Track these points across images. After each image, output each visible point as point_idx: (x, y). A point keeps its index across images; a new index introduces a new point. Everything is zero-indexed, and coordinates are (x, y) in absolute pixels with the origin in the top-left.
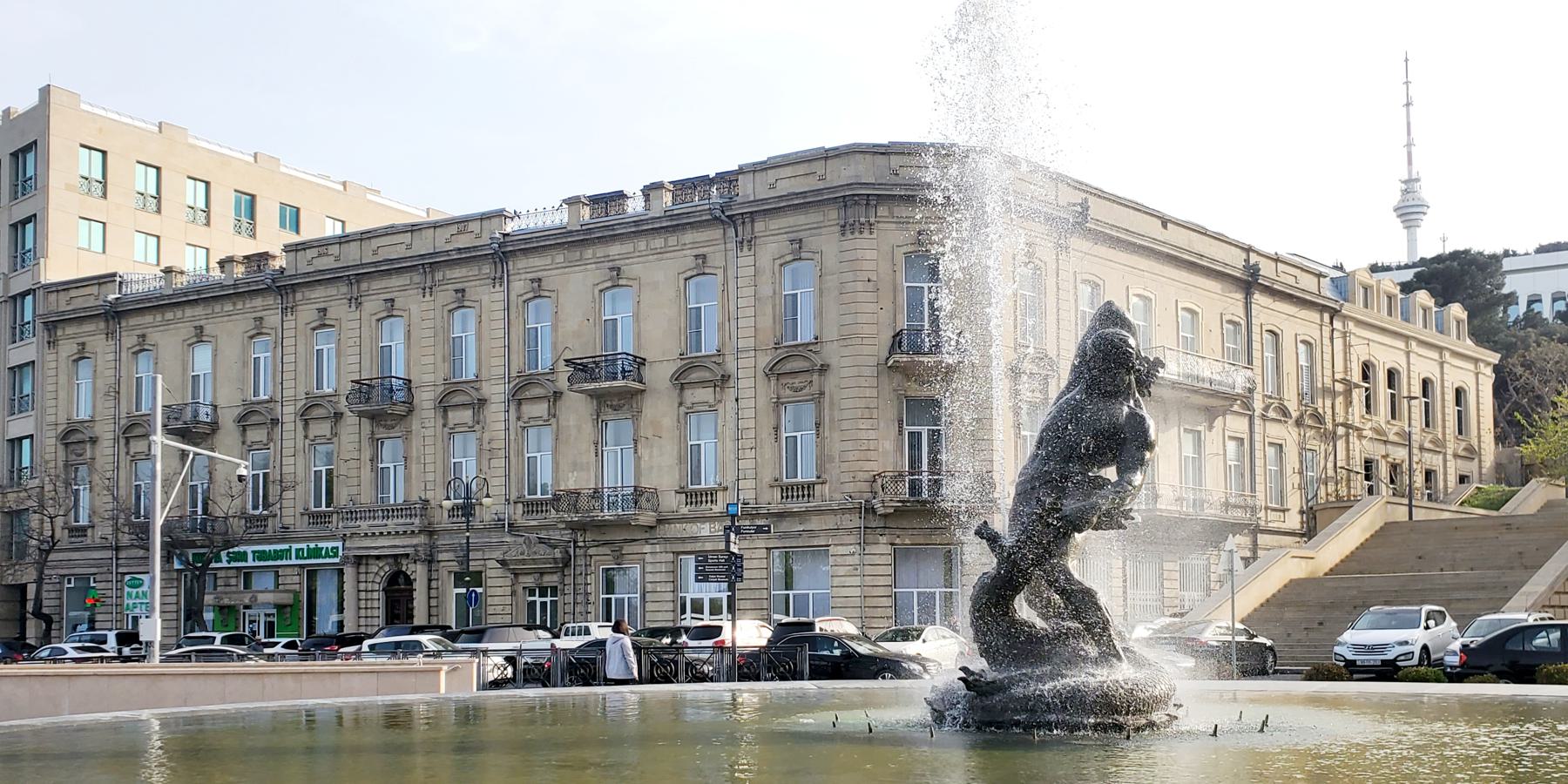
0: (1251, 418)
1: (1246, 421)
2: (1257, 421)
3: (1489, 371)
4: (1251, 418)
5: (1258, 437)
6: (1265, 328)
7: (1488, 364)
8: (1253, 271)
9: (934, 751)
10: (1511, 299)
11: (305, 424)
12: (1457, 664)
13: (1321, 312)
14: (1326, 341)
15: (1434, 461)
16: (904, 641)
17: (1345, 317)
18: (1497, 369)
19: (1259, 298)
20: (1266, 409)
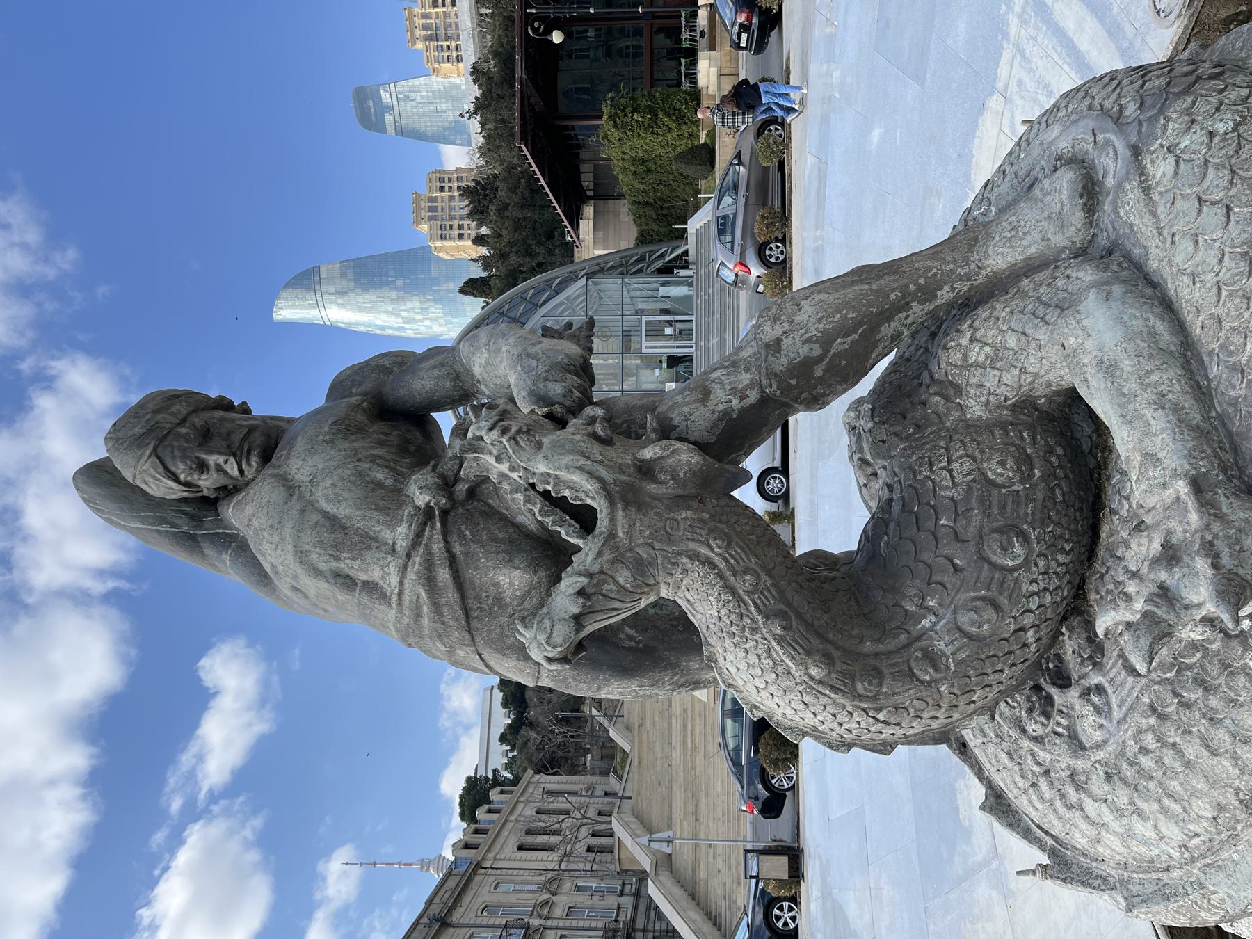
0: (545, 928)
1: (548, 932)
2: (549, 923)
3: (537, 777)
4: (545, 928)
5: (561, 924)
6: (479, 914)
7: (532, 776)
8: (436, 919)
9: (993, 770)
10: (484, 137)
11: (1139, 816)
12: (697, 571)
13: (475, 874)
14: (498, 872)
15: (591, 813)
16: (797, 756)
17: (483, 859)
18: (538, 772)
19: (456, 917)
20: (540, 916)
